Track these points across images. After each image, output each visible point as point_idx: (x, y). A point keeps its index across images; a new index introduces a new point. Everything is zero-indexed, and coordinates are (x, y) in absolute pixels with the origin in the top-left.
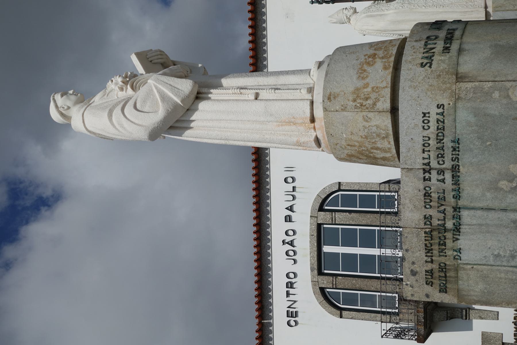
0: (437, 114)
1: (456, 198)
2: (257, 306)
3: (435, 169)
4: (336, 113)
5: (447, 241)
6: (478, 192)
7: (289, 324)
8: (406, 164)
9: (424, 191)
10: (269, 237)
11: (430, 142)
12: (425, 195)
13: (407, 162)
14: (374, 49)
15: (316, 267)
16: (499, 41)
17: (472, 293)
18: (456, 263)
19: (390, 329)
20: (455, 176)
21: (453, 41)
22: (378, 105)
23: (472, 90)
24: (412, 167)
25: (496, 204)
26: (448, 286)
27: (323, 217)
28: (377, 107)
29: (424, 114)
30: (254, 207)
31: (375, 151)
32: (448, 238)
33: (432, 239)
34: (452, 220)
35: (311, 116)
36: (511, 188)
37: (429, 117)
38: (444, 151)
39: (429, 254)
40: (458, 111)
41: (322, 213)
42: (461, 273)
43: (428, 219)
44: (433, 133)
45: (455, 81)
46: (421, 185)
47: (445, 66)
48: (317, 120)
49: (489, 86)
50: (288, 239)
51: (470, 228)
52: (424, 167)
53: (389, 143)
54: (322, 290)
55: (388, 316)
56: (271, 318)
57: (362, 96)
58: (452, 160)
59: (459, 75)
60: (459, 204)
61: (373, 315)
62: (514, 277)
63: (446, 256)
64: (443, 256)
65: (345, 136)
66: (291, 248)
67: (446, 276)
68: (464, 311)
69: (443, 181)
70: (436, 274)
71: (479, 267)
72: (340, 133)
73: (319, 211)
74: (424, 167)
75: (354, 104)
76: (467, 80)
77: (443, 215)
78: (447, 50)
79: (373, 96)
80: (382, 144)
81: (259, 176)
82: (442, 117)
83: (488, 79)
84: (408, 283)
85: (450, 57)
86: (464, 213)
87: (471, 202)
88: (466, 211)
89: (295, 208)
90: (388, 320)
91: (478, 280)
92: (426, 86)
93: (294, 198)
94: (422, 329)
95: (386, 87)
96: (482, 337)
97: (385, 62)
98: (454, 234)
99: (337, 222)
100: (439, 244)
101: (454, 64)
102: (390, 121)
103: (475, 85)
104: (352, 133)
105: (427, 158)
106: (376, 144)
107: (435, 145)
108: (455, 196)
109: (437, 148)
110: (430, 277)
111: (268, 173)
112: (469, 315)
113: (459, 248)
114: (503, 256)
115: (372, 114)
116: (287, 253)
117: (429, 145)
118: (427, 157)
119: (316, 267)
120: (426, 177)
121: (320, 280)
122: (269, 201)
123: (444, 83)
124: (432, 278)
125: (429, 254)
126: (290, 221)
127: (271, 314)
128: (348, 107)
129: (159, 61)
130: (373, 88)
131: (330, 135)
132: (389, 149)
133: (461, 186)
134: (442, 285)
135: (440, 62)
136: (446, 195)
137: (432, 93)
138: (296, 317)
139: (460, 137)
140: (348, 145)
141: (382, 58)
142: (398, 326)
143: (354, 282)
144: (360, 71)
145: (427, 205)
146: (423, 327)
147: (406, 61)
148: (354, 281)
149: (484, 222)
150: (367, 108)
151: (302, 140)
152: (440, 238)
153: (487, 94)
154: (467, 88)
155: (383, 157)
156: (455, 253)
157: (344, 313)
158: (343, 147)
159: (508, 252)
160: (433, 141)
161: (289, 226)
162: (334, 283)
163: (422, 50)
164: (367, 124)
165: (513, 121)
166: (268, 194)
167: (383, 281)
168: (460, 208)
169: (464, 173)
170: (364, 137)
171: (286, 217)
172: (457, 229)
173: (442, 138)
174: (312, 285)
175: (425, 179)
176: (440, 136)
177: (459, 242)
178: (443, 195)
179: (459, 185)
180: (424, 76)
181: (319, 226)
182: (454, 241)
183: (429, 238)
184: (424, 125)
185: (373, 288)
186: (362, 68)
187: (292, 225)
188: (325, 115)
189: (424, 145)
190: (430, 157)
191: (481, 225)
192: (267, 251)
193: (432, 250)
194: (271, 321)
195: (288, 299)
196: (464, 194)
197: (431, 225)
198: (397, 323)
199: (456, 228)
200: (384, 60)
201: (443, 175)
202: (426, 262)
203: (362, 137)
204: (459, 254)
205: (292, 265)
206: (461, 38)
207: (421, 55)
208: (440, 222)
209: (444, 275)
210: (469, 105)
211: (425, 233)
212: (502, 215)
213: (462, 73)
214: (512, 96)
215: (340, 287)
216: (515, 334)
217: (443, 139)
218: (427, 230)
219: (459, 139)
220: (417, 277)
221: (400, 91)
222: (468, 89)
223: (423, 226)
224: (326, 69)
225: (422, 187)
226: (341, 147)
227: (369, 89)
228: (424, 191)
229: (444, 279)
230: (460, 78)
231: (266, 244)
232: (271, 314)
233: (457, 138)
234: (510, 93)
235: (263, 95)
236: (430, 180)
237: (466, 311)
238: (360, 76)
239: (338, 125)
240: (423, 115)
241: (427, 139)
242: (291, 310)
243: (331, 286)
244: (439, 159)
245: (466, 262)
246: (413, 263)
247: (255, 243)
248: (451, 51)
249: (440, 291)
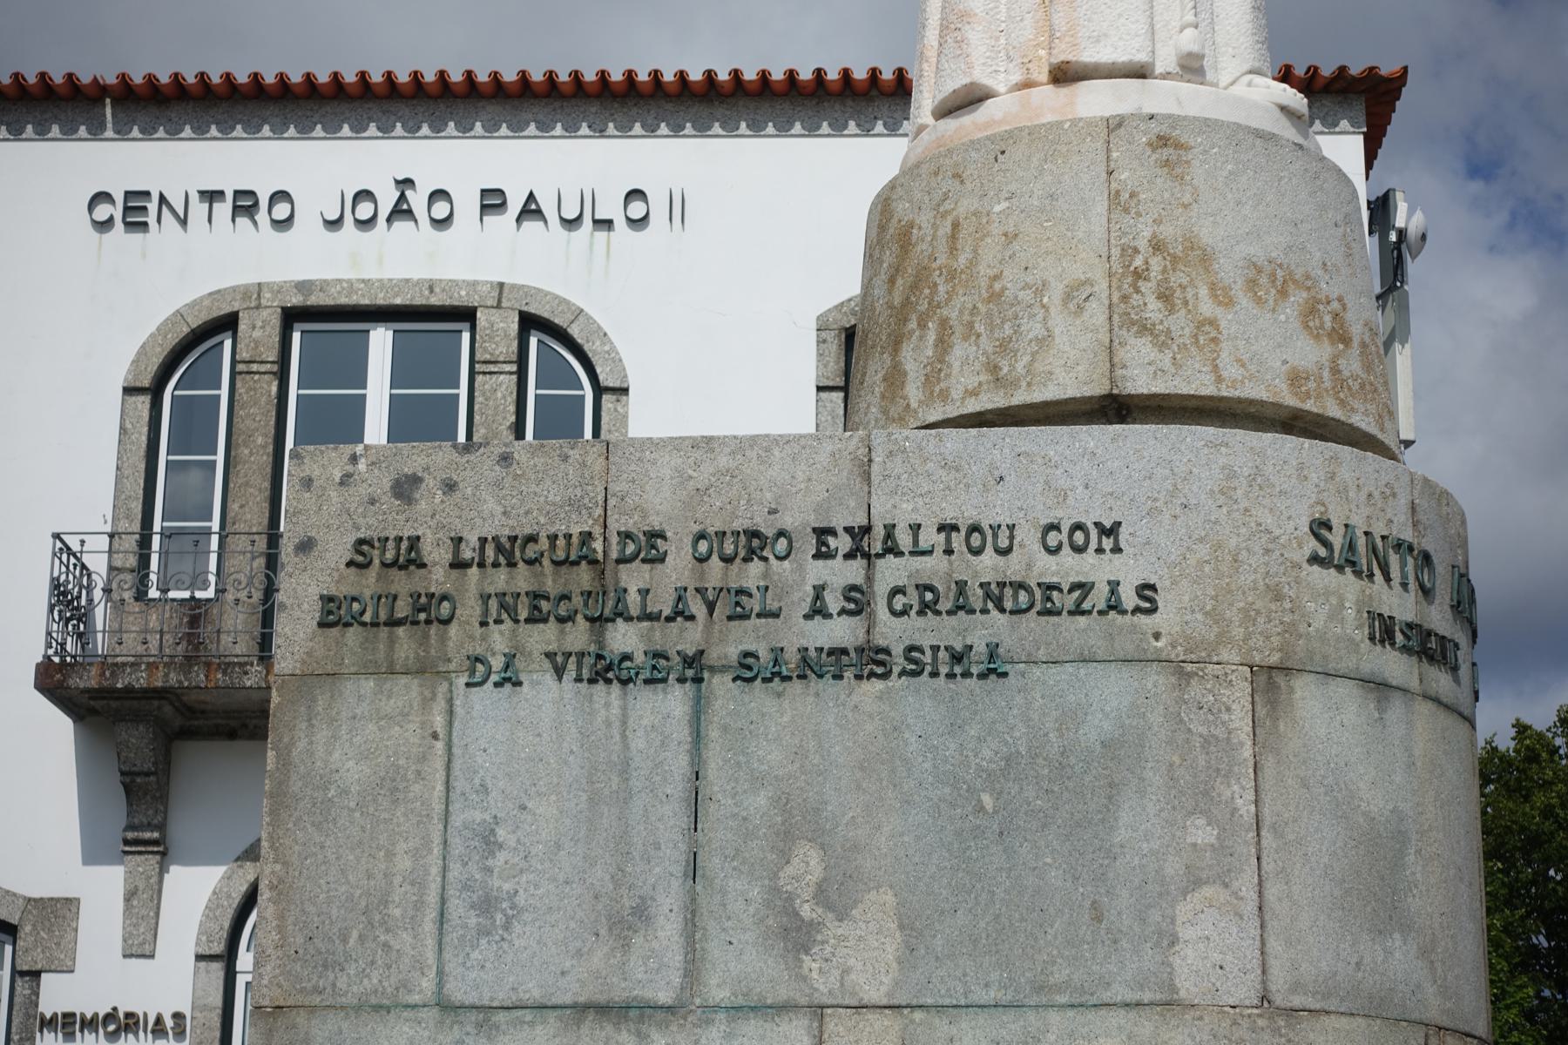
0: (1114, 586)
2: (164, 79)
3: (869, 579)
5: (551, 628)
6: (771, 756)
7: (102, 197)
9: (770, 532)
10: (425, 130)
11: (989, 556)
12: (754, 534)
13: (899, 460)
14: (1367, 340)
16: (1418, 852)
17: (322, 735)
18: (452, 666)
19: (84, 567)
20: (838, 660)
21: (1415, 658)
22: (1140, 342)
23: (1220, 732)
24: (875, 479)
25: (718, 832)
26: (353, 635)
27: (499, 329)
28: (1132, 341)
30: (537, 76)
31: (931, 337)
32: (562, 632)
33: (556, 563)
34: (642, 647)
35: (1086, 65)
36: (790, 898)
37: (1100, 551)
38: (949, 613)
39: (490, 552)
40: (1126, 671)
41: (516, 326)
43: (649, 546)
44: (1029, 566)
45: (1257, 659)
46: (798, 517)
47: (1319, 622)
48: (1064, 92)
49: (1239, 802)
50: (417, 200)
51: (608, 724)
52: (879, 532)
53: (974, 393)
54: (228, 323)
55: (132, 561)
56: (122, 133)
57: (1178, 278)
58: (911, 648)
59: (1280, 679)
60: (716, 679)
61: (137, 507)
62: (397, 912)
63: (483, 624)
64: (486, 612)
65: (997, 208)
66: (385, 209)
67: (393, 623)
68: (156, 835)
69: (818, 610)
70: (402, 584)
71: (439, 764)
72: (1013, 187)
73: (521, 313)
74: (879, 532)
76: (1262, 712)
77: (667, 612)
78: (1384, 630)
79: (1180, 324)
80: (965, 361)
81: (652, 96)
82: (1102, 605)
83: (1266, 799)
84: (362, 466)
85: (1353, 645)
86: (675, 700)
87: (725, 729)
88: (687, 709)
89: (531, 226)
90: (118, 563)
91: (382, 759)
92: (1233, 542)
93: (571, 224)
94: (89, 680)
95: (1219, 379)
96: (58, 900)
98: (581, 655)
99: (479, 379)
100: (536, 596)
101: (1325, 657)
102: (1072, 392)
103: (1242, 744)
104: (1011, 238)
105: (916, 542)
106: (966, 338)
107: (976, 574)
108: (750, 661)
109: (961, 586)
110: (389, 556)
111: (664, 129)
112: (140, 853)
113: (523, 677)
114: (490, 862)
115: (1101, 319)
116: (364, 195)
117: (977, 552)
118: (924, 544)
119: (315, 300)
120: (832, 541)
121: (265, 313)
122: (559, 130)
123: (1249, 616)
124: (384, 565)
125: (490, 552)
126: (483, 207)
127: (136, 132)
128: (1128, 220)
130: (1213, 322)
131: (1000, 146)
132: (945, 396)
133: (797, 685)
134: (356, 606)
136: (754, 621)
137: (1201, 563)
138: (128, 225)
140: (956, 226)
141: (1335, 371)
142: (98, 594)
143: (260, 440)
144: (1280, 273)
145: (712, 544)
146: (93, 684)
147: (1334, 458)
148: (263, 439)
149: (636, 784)
150: (1125, 298)
151: (975, 36)
152: (566, 597)
153: (1206, 793)
154: (1228, 709)
155: (905, 374)
156: (497, 663)
157: (143, 403)
158: (947, 206)
159: (507, 886)
160: (995, 569)
161: (467, 204)
162: (255, 367)
163: (1379, 529)
164: (1054, 297)
165: (1087, 904)
166: (584, 130)
167: (262, 543)
168: (698, 680)
169: (855, 698)
170: (997, 286)
171: (500, 192)
172: (606, 670)
173: (1008, 605)
174: (246, 286)
175: (823, 533)
176: (1015, 597)
177: (549, 678)
178: (757, 609)
179: (802, 677)
180: (1277, 532)
181: (466, 315)
182: (550, 656)
183: (561, 555)
184: (1065, 528)
185: (235, 506)
186: (1295, 282)
187: (465, 218)
188: (1090, 123)
189: (975, 528)
190: (923, 553)
191: (625, 769)
192: (371, 119)
193: (512, 564)
194: (109, 133)
195: (194, 198)
196: (759, 697)
197: (618, 561)
198: (107, 591)
199: (609, 668)
200: (1326, 374)
201: (843, 612)
202: (457, 541)
203: (996, 278)
204: (494, 678)
205: (323, 215)
206: (1426, 697)
208: (633, 598)
209: (400, 615)
210: (1156, 718)
211: (587, 537)
212: (672, 857)
213: (1291, 690)
214: (1196, 898)
215: (241, 388)
216: (73, 1015)
217: (1002, 611)
218: (598, 545)
219: (1005, 675)
220: (389, 502)
221: (1211, 430)
222: (1225, 717)
223: (614, 526)
225: (788, 521)
226: (946, 197)
227: (1207, 308)
228: (770, 532)
229: (383, 616)
230: (1270, 679)
231: (399, 119)
232: (136, 132)
233: (1007, 668)
234: (1208, 891)
236: (818, 556)
237: (155, 842)
239: (1048, 178)
240: (1108, 524)
241: (1003, 542)
242: (153, 207)
243: (244, 354)
244: (912, 591)
246: (450, 487)
247: (403, 77)
248: (1379, 648)
249: (328, 599)
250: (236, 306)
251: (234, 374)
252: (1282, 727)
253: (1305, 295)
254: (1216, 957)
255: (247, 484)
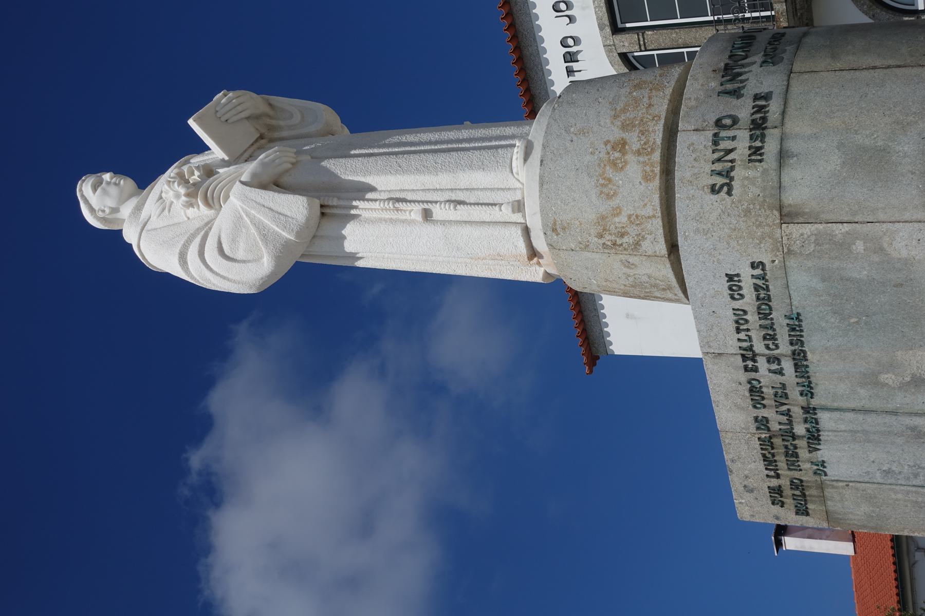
1: (806, 395)
3: (763, 355)
4: (571, 252)
8: (710, 347)
9: (749, 386)
12: (751, 390)
15: (607, 22)
17: (851, 516)
23: (813, 238)
25: (878, 404)
26: (810, 506)
28: (644, 248)
29: (730, 278)
33: (773, 448)
35: (527, 247)
42: (828, 492)
45: (778, 221)
47: (758, 191)
59: (785, 211)
63: (801, 470)
64: (796, 470)
67: (804, 495)
69: (780, 372)
70: (788, 492)
71: (859, 485)
75: (601, 241)
76: (801, 220)
78: (756, 153)
79: (633, 231)
83: (840, 219)
85: (765, 172)
87: (833, 401)
92: (726, 230)
95: (654, 216)
97: (644, 162)
100: (787, 455)
121: (616, 42)
129: (243, 115)
135: (746, 182)
139: (799, 311)
144: (602, 181)
148: (673, 34)
149: (860, 429)
154: (802, 235)
162: (642, 43)
168: (814, 409)
172: (814, 437)
200: (641, 159)
201: (779, 364)
206: (783, 124)
207: (708, 167)
213: (790, 205)
215: (653, 47)
218: (763, 436)
222: (805, 236)
224: (538, 171)
228: (749, 386)
230: (787, 216)
235: (439, 212)
238: (601, 193)
245: (836, 478)
249: (797, 513)
250: (616, 54)
251: (646, 50)
252: (807, 210)
253: (608, 168)
254: (914, 242)
255: (695, 38)
